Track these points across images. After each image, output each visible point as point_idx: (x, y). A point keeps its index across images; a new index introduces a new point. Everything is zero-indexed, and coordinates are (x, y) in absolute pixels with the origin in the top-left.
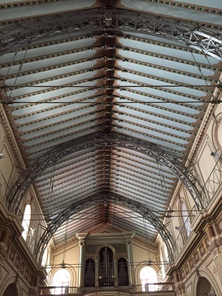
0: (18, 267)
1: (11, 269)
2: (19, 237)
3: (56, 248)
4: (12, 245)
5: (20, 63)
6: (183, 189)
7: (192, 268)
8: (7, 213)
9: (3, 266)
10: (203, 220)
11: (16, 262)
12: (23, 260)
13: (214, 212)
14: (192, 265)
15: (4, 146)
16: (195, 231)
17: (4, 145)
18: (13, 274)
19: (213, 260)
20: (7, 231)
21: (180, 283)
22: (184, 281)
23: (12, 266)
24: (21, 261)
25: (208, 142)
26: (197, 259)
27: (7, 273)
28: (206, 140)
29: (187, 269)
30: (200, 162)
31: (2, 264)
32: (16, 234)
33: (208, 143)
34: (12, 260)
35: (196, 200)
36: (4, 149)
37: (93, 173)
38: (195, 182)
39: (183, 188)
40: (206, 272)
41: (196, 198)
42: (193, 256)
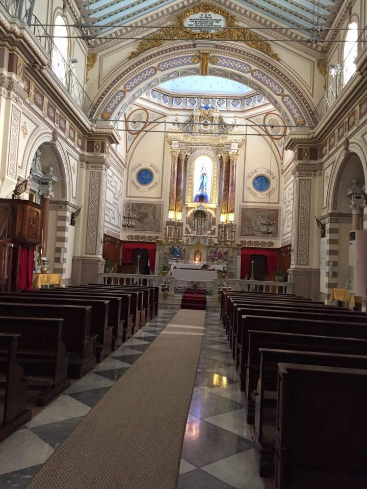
0: (53, 120)
2: (43, 69)
7: (340, 138)
8: (8, 21)
20: (16, 53)
24: (57, 111)
26: (351, 123)
27: (35, 126)
32: (37, 63)
40: (360, 144)
42: (347, 119)
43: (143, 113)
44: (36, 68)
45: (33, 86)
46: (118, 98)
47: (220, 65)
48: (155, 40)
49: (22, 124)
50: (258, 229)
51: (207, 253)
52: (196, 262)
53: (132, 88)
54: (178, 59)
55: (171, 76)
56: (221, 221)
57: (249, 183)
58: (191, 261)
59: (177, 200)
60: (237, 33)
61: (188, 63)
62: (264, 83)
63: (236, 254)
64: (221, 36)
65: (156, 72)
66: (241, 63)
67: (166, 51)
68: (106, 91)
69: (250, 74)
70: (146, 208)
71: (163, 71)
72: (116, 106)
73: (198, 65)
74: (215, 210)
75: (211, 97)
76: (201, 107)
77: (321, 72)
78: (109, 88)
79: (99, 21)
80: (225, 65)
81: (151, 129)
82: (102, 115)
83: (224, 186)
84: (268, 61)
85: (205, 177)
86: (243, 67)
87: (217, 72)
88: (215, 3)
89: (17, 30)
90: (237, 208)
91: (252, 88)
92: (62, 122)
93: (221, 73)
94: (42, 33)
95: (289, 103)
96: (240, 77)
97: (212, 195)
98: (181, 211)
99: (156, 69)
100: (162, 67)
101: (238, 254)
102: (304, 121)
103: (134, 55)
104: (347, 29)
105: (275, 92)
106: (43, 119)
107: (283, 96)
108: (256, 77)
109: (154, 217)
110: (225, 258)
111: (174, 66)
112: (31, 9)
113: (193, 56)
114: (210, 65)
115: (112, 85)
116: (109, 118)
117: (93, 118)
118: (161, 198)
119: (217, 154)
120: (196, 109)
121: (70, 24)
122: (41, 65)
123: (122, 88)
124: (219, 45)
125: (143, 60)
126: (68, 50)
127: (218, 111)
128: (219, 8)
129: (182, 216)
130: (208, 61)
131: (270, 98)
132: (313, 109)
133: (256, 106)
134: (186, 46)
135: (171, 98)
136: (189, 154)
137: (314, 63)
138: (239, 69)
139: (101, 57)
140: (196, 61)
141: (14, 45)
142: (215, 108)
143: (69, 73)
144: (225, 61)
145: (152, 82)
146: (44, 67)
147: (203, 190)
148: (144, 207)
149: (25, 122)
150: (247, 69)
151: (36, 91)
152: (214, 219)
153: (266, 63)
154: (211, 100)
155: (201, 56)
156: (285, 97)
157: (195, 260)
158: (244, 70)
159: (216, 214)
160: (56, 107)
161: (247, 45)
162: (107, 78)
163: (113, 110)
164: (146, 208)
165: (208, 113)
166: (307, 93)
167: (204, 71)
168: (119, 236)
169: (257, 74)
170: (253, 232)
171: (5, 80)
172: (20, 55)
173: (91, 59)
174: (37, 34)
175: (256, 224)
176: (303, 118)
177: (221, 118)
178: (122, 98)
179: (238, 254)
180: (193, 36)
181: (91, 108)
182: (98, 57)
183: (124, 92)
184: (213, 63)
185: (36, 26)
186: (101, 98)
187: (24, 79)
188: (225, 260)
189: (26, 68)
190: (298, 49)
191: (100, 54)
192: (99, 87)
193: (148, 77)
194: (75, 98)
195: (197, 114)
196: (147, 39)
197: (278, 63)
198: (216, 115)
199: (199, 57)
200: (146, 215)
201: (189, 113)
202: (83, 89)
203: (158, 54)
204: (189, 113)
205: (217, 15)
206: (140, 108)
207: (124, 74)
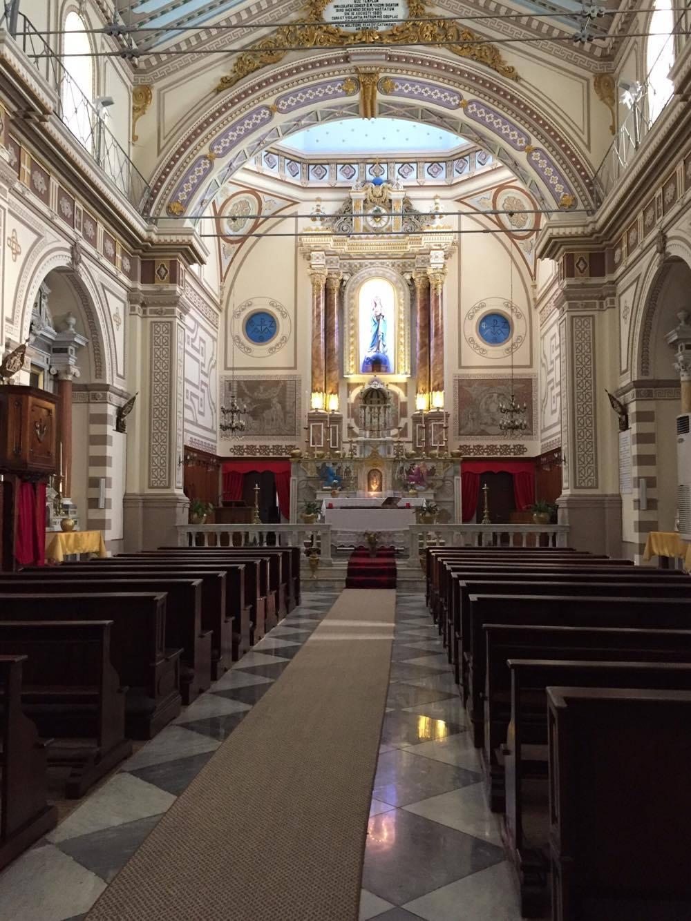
0: (71, 221)
1: (47, 227)
2: (45, 121)
4: (119, 240)
7: (647, 229)
12: (124, 241)
13: (633, 191)
14: (648, 221)
18: (59, 241)
24: (77, 204)
26: (668, 198)
29: (632, 234)
31: (6, 206)
32: (31, 109)
34: (45, 198)
36: (107, 64)
42: (660, 191)
43: (247, 198)
47: (401, 94)
48: (268, 52)
49: (9, 234)
50: (493, 420)
51: (393, 473)
52: (372, 493)
53: (226, 151)
54: (314, 87)
55: (303, 122)
56: (419, 408)
57: (471, 328)
58: (360, 492)
59: (328, 371)
61: (336, 95)
62: (490, 126)
63: (451, 473)
65: (271, 115)
66: (442, 90)
68: (174, 160)
69: (461, 110)
70: (265, 390)
72: (196, 187)
73: (356, 98)
74: (405, 386)
75: (384, 161)
76: (366, 182)
77: (602, 99)
78: (179, 153)
79: (152, 18)
82: (169, 207)
83: (421, 337)
85: (381, 321)
90: (450, 371)
92: (89, 226)
96: (441, 116)
97: (397, 356)
98: (337, 393)
99: (272, 111)
100: (283, 105)
101: (456, 472)
102: (575, 199)
103: (226, 83)
105: (513, 144)
106: (49, 221)
108: (473, 116)
109: (284, 408)
110: (430, 482)
113: (345, 79)
114: (380, 97)
115: (185, 146)
116: (182, 212)
117: (151, 215)
118: (295, 368)
119: (403, 273)
120: (357, 186)
123: (205, 151)
125: (246, 94)
126: (93, 79)
127: (401, 188)
129: (340, 402)
130: (376, 88)
131: (503, 156)
132: (591, 175)
134: (329, 61)
135: (305, 166)
136: (346, 278)
139: (160, 90)
140: (351, 90)
144: (410, 86)
145: (265, 136)
146: (48, 117)
147: (378, 348)
148: (261, 388)
151: (34, 167)
152: (404, 404)
154: (385, 166)
156: (534, 154)
157: (370, 489)
158: (449, 102)
159: (406, 395)
163: (191, 195)
164: (265, 390)
165: (380, 193)
166: (577, 142)
167: (367, 110)
168: (214, 448)
169: (475, 110)
170: (483, 427)
173: (141, 96)
174: (29, 51)
175: (488, 410)
176: (572, 193)
178: (207, 172)
179: (456, 472)
181: (146, 196)
182: (154, 92)
183: (210, 158)
188: (431, 486)
189: (12, 121)
192: (159, 152)
193: (256, 127)
194: (113, 176)
198: (396, 195)
199: (357, 82)
200: (267, 405)
201: (343, 195)
202: (128, 158)
203: (275, 79)
204: (343, 195)
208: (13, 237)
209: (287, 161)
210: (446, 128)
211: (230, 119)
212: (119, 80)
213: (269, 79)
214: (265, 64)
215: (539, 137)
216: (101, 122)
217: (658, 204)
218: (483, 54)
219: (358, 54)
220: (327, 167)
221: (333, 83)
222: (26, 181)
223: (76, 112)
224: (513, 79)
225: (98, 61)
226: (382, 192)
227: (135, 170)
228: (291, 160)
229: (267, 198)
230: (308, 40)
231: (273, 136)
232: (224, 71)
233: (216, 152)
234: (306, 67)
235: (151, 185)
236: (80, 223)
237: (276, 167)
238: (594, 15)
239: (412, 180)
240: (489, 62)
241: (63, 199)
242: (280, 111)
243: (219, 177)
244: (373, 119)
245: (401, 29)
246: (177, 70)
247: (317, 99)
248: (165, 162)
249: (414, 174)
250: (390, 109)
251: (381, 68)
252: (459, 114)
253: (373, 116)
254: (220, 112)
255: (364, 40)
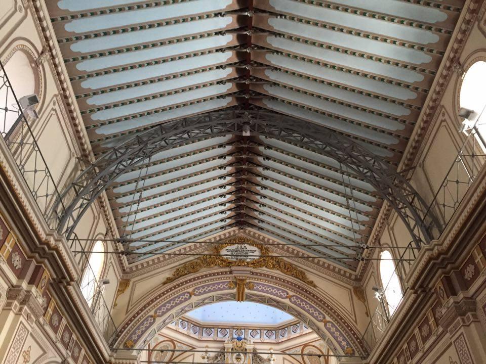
0: (66, 346)
2: (70, 285)
3: (131, 268)
5: (136, 181)
6: (386, 229)
9: (31, 334)
10: (431, 263)
11: (63, 335)
13: (408, 316)
15: (53, 112)
16: (413, 288)
17: (55, 110)
18: (56, 357)
19: (451, 344)
20: (43, 266)
21: (461, 296)
22: (472, 290)
23: (55, 341)
24: (74, 336)
25: (445, 121)
26: (412, 349)
28: (441, 118)
30: (427, 162)
32: (64, 278)
33: (444, 124)
34: (55, 330)
35: (416, 232)
37: (222, 200)
38: (413, 199)
39: (387, 226)
41: (414, 228)
42: (406, 345)
43: (168, 344)
44: (62, 284)
45: (53, 304)
46: (146, 324)
47: (257, 290)
48: (192, 267)
49: (25, 348)
53: (164, 313)
54: (214, 285)
55: (206, 301)
60: (272, 261)
61: (224, 289)
62: (303, 308)
64: (255, 264)
65: (190, 296)
66: (278, 289)
67: (202, 277)
68: (134, 317)
69: (288, 299)
71: (198, 295)
72: (143, 332)
73: (235, 291)
75: (243, 328)
76: (233, 338)
77: (359, 299)
78: (138, 313)
79: (138, 249)
80: (262, 291)
81: (182, 360)
82: (125, 343)
84: (305, 287)
86: (280, 293)
87: (255, 297)
88: (249, 237)
89: (52, 242)
91: (292, 314)
92: (77, 350)
93: (258, 298)
94: (79, 249)
95: (333, 330)
96: (278, 302)
99: (190, 294)
100: (197, 292)
102: (353, 350)
103: (169, 280)
104: (379, 259)
105: (316, 318)
106: (54, 344)
107: (326, 323)
108: (295, 303)
111: (210, 291)
112: (73, 227)
113: (230, 282)
114: (246, 291)
115: (141, 310)
116: (132, 346)
117: (114, 347)
120: (228, 341)
121: (109, 251)
122: (69, 280)
123: (152, 313)
124: (255, 272)
125: (179, 286)
126: (101, 273)
127: (252, 343)
128: (253, 241)
130: (245, 286)
131: (311, 324)
132: (360, 337)
133: (291, 338)
134: (222, 273)
135: (201, 329)
137: (350, 290)
138: (276, 295)
139: (134, 282)
140: (232, 287)
141: (44, 258)
142: (249, 339)
143: (98, 294)
144: (262, 288)
145: (185, 307)
146: (73, 283)
149: (30, 347)
150: (284, 295)
151: (55, 311)
153: (303, 289)
154: (243, 331)
155: (238, 282)
156: (328, 324)
158: (282, 295)
160: (73, 331)
161: (282, 272)
162: (141, 300)
163: (139, 337)
165: (241, 345)
166: (350, 320)
167: (240, 297)
169: (295, 300)
171: (22, 293)
172: (48, 269)
173: (124, 284)
174: (73, 249)
176: (351, 347)
177: (254, 350)
178: (151, 324)
180: (229, 264)
181: (114, 336)
182: (131, 283)
183: (154, 318)
184: (250, 289)
185: (75, 241)
186: (128, 324)
187: (45, 294)
189: (51, 284)
190: (332, 277)
191: (133, 280)
192: (127, 313)
193: (181, 302)
194: (98, 322)
195: (229, 346)
196: (185, 266)
197: (314, 289)
198: (249, 347)
199: (236, 283)
201: (221, 345)
202: (110, 313)
203: (194, 279)
204: (221, 345)
205: (252, 247)
206: (167, 339)
207: (156, 298)
208: (28, 351)
209: (192, 325)
210: (279, 308)
211: (168, 297)
212: (114, 274)
213: (191, 279)
214: (190, 273)
215: (329, 315)
216: (100, 292)
217: (406, 353)
218: (298, 274)
219: (235, 270)
220: (212, 329)
221: (223, 283)
222: (4, 254)
223: (89, 283)
224: (313, 286)
225: (107, 256)
226: (242, 344)
227: (111, 320)
228: (195, 325)
229: (179, 345)
230: (212, 263)
231: (190, 307)
232: (169, 274)
233: (158, 314)
234: (210, 275)
235: (118, 330)
236: (71, 348)
237: (186, 328)
238: (365, 247)
239: (257, 339)
240: (301, 278)
241: (66, 332)
242: (195, 295)
243: (157, 327)
244: (239, 302)
245: (257, 261)
246: (145, 273)
247: (215, 290)
248: (129, 318)
249: (258, 336)
250: (251, 297)
251: (247, 277)
252: (287, 301)
253: (242, 300)
254: (163, 294)
255: (240, 264)
